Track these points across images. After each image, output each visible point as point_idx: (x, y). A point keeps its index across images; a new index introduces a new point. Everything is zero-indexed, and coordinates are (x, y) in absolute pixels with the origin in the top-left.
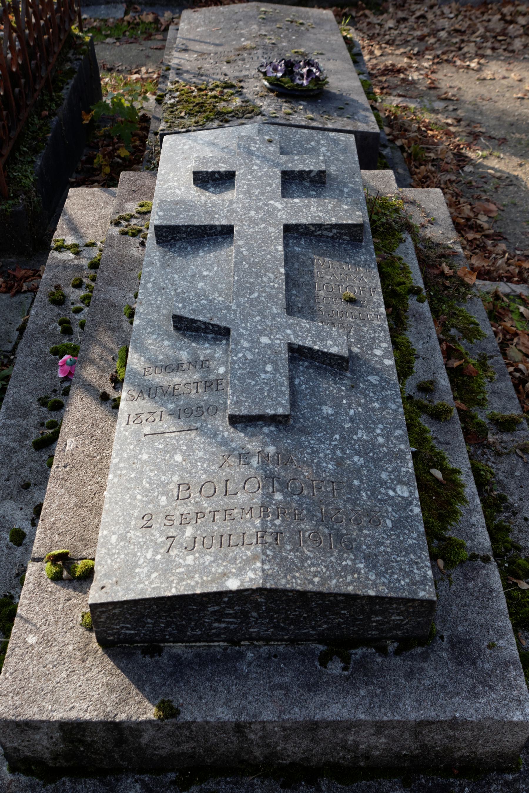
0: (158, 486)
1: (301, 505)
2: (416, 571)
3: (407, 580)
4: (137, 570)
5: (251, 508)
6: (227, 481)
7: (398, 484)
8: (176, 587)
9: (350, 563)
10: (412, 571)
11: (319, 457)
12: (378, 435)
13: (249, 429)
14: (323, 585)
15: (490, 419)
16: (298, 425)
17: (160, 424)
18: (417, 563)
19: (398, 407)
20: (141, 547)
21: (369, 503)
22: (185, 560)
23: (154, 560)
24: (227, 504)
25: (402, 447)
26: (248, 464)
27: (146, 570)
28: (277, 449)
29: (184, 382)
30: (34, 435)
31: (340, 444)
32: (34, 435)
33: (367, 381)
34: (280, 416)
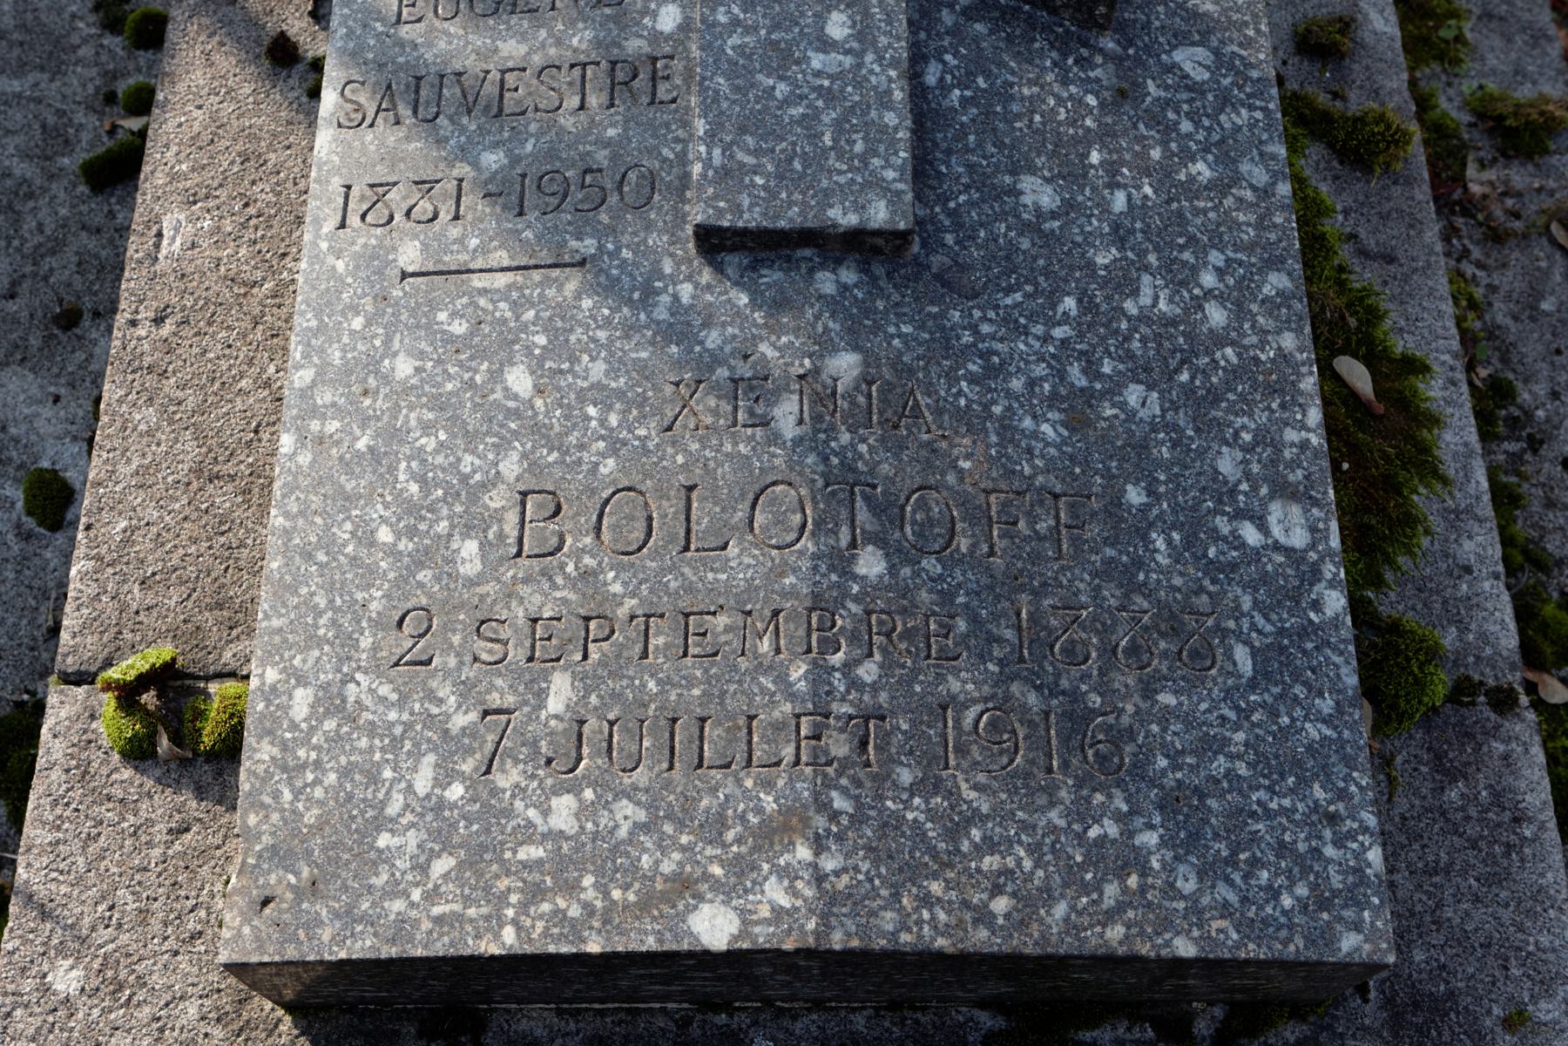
0: (451, 496)
1: (947, 597)
2: (1330, 851)
3: (1302, 890)
4: (384, 840)
5: (776, 613)
6: (690, 489)
7: (1272, 497)
8: (515, 922)
9: (1112, 829)
10: (1316, 852)
11: (1009, 394)
12: (1208, 294)
13: (771, 277)
14: (1023, 924)
15: (1474, 112)
16: (938, 260)
17: (455, 232)
18: (1333, 819)
19: (1275, 176)
20: (396, 743)
21: (1178, 581)
22: (546, 813)
23: (441, 805)
24: (689, 589)
25: (1288, 341)
26: (765, 423)
27: (412, 839)
28: (866, 364)
29: (537, 60)
30: (85, 137)
31: (1081, 335)
32: (85, 137)
33: (1173, 68)
34: (878, 233)
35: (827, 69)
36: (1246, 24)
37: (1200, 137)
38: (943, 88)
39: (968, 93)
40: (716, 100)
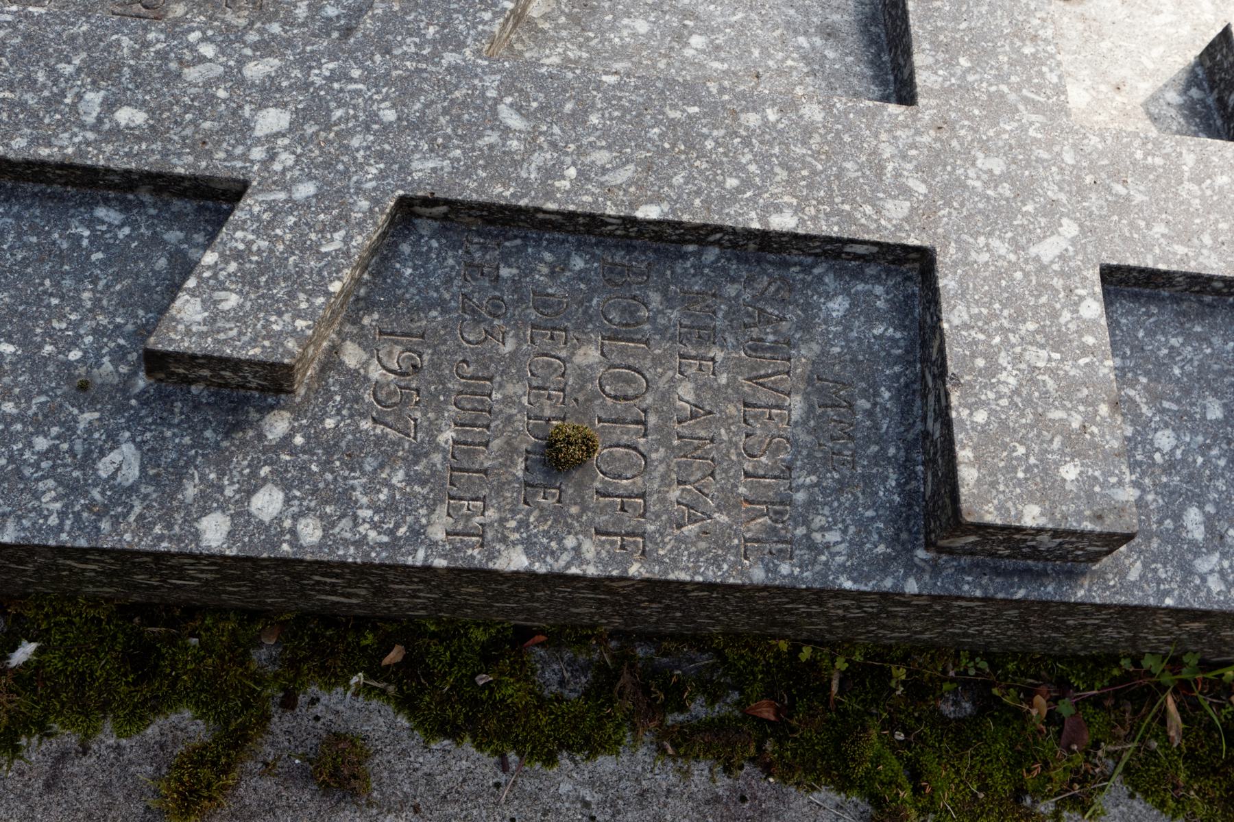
35: (82, 103)
36: (169, 526)
37: (27, 455)
38: (91, 221)
39: (85, 243)
40: (63, 22)
